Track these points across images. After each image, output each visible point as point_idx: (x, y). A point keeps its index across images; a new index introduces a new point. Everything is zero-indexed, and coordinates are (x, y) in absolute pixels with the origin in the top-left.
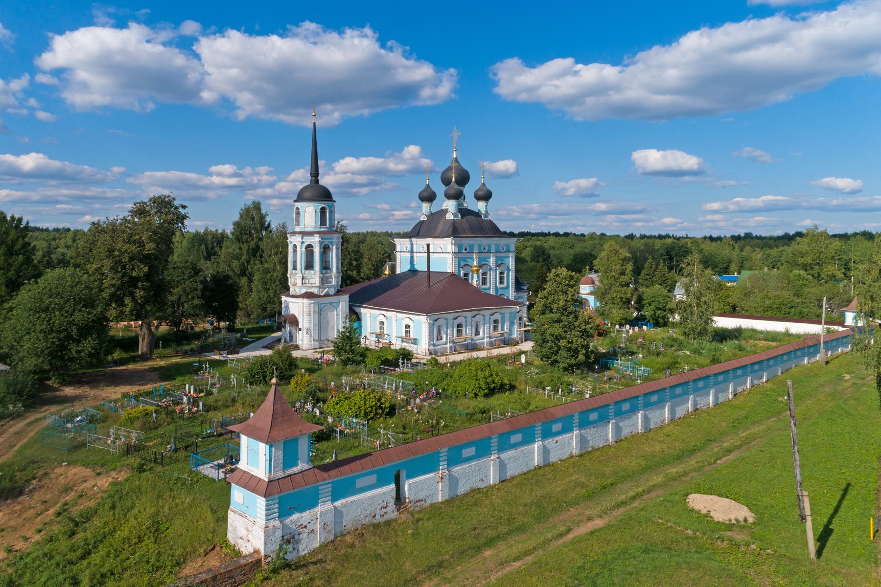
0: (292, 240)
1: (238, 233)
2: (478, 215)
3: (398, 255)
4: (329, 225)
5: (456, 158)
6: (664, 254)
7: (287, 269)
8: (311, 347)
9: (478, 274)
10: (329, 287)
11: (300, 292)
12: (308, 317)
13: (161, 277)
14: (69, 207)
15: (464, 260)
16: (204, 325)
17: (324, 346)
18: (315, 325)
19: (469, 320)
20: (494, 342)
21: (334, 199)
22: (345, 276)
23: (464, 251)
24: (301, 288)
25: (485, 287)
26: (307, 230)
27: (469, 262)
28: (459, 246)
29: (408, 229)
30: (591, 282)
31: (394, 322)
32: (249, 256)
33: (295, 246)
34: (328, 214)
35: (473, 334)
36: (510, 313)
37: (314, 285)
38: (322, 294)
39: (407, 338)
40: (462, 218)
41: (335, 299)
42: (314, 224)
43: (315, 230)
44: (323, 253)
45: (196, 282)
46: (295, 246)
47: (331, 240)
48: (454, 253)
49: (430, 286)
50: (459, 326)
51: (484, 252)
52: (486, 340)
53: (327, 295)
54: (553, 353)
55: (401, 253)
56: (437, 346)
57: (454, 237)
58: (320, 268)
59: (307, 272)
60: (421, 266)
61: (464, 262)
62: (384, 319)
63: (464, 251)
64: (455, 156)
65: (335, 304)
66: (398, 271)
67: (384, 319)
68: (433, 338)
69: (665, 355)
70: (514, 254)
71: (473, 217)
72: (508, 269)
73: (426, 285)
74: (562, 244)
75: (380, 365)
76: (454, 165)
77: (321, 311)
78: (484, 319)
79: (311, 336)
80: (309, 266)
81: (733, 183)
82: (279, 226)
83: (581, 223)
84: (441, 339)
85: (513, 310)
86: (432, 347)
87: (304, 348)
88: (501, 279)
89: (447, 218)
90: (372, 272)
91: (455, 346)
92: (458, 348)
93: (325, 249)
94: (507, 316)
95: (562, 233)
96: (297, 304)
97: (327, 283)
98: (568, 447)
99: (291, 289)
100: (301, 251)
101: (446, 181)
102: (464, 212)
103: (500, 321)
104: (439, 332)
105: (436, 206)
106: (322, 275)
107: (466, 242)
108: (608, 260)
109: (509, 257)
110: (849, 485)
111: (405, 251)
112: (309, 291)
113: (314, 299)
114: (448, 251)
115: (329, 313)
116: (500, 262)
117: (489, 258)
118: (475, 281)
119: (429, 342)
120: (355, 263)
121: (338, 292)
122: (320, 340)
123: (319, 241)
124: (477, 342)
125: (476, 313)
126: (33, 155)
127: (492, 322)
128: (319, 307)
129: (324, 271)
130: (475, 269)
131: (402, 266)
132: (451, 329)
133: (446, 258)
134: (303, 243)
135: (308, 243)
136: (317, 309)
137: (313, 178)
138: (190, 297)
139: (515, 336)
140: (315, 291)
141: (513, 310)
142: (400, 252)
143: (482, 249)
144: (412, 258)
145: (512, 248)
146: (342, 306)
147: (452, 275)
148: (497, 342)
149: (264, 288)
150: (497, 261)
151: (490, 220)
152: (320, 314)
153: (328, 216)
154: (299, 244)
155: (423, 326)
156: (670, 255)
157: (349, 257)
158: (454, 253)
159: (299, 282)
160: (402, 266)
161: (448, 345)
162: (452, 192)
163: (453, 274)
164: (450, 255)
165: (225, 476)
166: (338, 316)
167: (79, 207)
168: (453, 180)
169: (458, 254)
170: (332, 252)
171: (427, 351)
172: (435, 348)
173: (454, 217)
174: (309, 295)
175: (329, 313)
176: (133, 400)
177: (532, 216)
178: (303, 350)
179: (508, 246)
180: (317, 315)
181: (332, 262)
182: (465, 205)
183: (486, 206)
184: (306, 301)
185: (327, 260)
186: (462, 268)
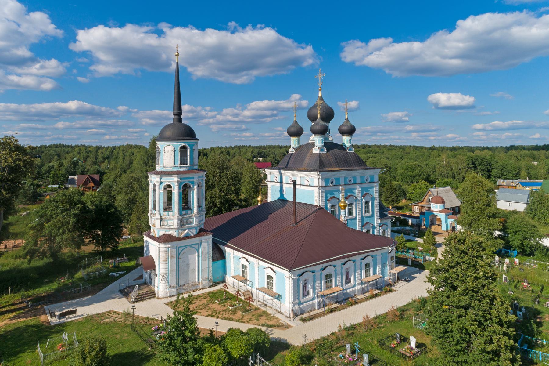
0: (152, 180)
2: (342, 147)
3: (269, 184)
4: (190, 164)
5: (321, 97)
6: (470, 163)
7: (243, 214)
8: (168, 295)
9: (345, 209)
10: (189, 228)
11: (158, 233)
12: (165, 262)
14: (97, 130)
15: (331, 193)
17: (183, 291)
18: (172, 271)
19: (338, 268)
20: (366, 289)
21: (197, 137)
22: (224, 200)
23: (331, 185)
24: (159, 230)
25: (351, 217)
27: (336, 194)
28: (326, 180)
30: (441, 201)
31: (256, 269)
33: (154, 185)
35: (344, 283)
37: (172, 227)
38: (181, 237)
39: (268, 290)
40: (327, 152)
41: (197, 240)
42: (173, 164)
43: (175, 170)
45: (70, 216)
46: (154, 185)
47: (192, 180)
48: (320, 187)
49: (296, 223)
50: (328, 276)
51: (350, 184)
52: (357, 287)
53: (187, 237)
54: (460, 351)
55: (272, 183)
56: (303, 303)
57: (320, 172)
58: (179, 210)
59: (166, 213)
60: (289, 197)
61: (331, 194)
62: (246, 264)
63: (331, 185)
64: (320, 95)
66: (269, 200)
67: (246, 264)
68: (299, 296)
70: (378, 184)
71: (337, 150)
72: (373, 199)
73: (293, 221)
74: (394, 156)
76: (319, 102)
77: (179, 254)
78: (355, 265)
79: (168, 283)
80: (168, 206)
81: (489, 113)
83: (397, 137)
84: (308, 294)
85: (385, 251)
86: (297, 307)
87: (160, 296)
88: (367, 208)
89: (314, 152)
90: (253, 190)
91: (323, 301)
92: (327, 301)
93: (185, 189)
94: (379, 258)
97: (187, 224)
101: (313, 118)
102: (329, 146)
103: (371, 265)
104: (305, 287)
105: (303, 140)
107: (332, 176)
108: (472, 191)
109: (373, 187)
111: (275, 181)
113: (171, 243)
114: (315, 185)
115: (190, 256)
116: (365, 193)
117: (355, 189)
118: (343, 216)
119: (294, 299)
120: (233, 188)
121: (201, 232)
122: (179, 286)
123: (178, 182)
124: (348, 291)
126: (76, 102)
127: (324, 277)
129: (184, 212)
130: (342, 204)
131: (272, 196)
132: (319, 282)
133: (313, 192)
134: (161, 183)
135: (167, 183)
136: (174, 253)
137: (176, 117)
138: (61, 231)
139: (387, 278)
140: (174, 233)
141: (385, 251)
142: (271, 181)
143: (348, 181)
144: (281, 188)
145: (376, 179)
146: (204, 247)
147: (319, 209)
148: (369, 288)
150: (362, 192)
152: (178, 258)
153: (189, 155)
155: (286, 281)
156: (475, 165)
157: (228, 183)
158: (320, 187)
160: (272, 196)
161: (316, 301)
162: (317, 128)
163: (320, 208)
167: (103, 131)
168: (319, 116)
169: (324, 188)
170: (193, 191)
171: (291, 312)
172: (301, 306)
173: (320, 151)
175: (190, 256)
177: (366, 134)
178: (159, 298)
179: (372, 177)
181: (193, 202)
182: (330, 139)
183: (350, 140)
186: (329, 201)
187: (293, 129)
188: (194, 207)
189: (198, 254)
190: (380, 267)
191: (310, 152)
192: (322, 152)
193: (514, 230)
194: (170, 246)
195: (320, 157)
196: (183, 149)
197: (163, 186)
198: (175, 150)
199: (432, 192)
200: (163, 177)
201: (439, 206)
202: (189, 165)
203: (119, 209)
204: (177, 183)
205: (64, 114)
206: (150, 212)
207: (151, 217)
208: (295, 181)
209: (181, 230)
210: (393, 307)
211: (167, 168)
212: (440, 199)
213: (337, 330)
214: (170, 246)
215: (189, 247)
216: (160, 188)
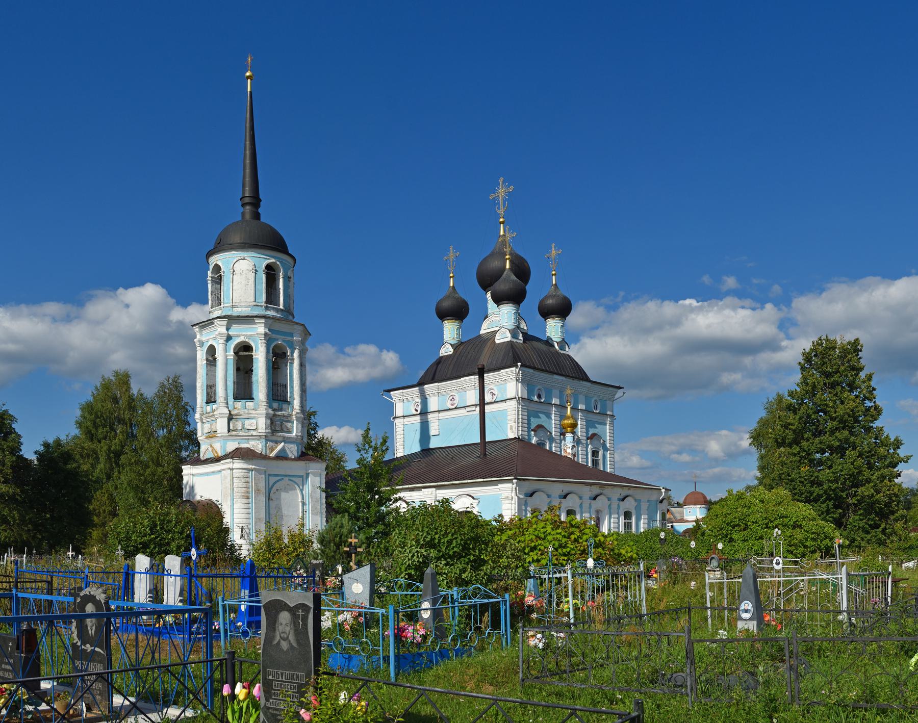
0: (204, 339)
1: (89, 424)
7: (307, 605)
10: (285, 440)
12: (244, 500)
13: (316, 546)
16: (264, 564)
18: (258, 520)
23: (536, 398)
26: (237, 312)
29: (416, 383)
30: (702, 500)
32: (111, 465)
33: (212, 350)
34: (281, 280)
36: (648, 501)
37: (255, 433)
38: (273, 455)
42: (252, 299)
43: (256, 313)
44: (274, 368)
47: (289, 338)
53: (282, 457)
55: (406, 419)
59: (239, 404)
65: (299, 480)
69: (101, 451)
75: (556, 342)
80: (243, 391)
82: (166, 383)
89: (497, 342)
94: (644, 506)
95: (260, 210)
96: (218, 476)
97: (282, 431)
98: (496, 591)
99: (203, 448)
100: (225, 357)
106: (271, 412)
109: (605, 424)
110: (623, 388)
112: (247, 340)
113: (255, 461)
125: (625, 492)
127: (622, 512)
128: (267, 481)
129: (275, 405)
134: (229, 338)
136: (262, 485)
140: (258, 446)
142: (404, 417)
149: (139, 499)
151: (568, 355)
152: (269, 499)
154: (222, 341)
159: (221, 425)
164: (514, 402)
165: (531, 577)
166: (306, 508)
168: (508, 266)
170: (292, 363)
174: (240, 454)
176: (333, 554)
180: (263, 498)
181: (292, 387)
184: (238, 464)
185: (281, 381)
187: (447, 304)
188: (294, 399)
189: (303, 499)
190: (646, 517)
191: (261, 681)
192: (515, 340)
193: (367, 678)
194: (253, 467)
195: (512, 347)
196: (270, 271)
197: (233, 346)
198: (256, 270)
199: (672, 514)
200: (234, 327)
201: (698, 509)
202: (281, 307)
203: (433, 504)
204: (263, 337)
205: (205, 668)
206: (198, 410)
207: (203, 423)
208: (103, 376)
209: (272, 441)
210: (804, 350)
211: (240, 309)
212: (701, 496)
213: (727, 495)
214: (253, 467)
215: (287, 479)
216: (226, 350)
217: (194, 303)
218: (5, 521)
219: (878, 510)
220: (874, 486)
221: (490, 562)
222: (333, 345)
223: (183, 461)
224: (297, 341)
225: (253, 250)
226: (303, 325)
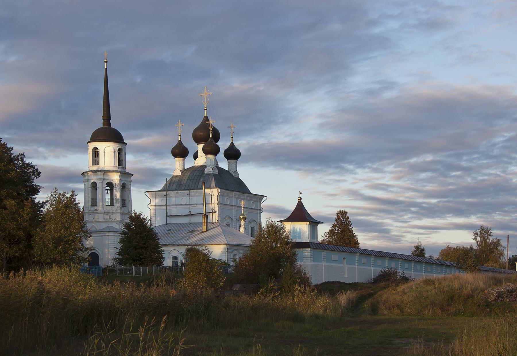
7: (98, 255)
42: (113, 164)
168: (211, 137)
217: (410, 254)
218: (210, 355)
219: (51, 289)
220: (59, 213)
221: (499, 302)
222: (214, 259)
223: (310, 222)
224: (150, 271)
225: (297, 166)
226: (266, 199)
